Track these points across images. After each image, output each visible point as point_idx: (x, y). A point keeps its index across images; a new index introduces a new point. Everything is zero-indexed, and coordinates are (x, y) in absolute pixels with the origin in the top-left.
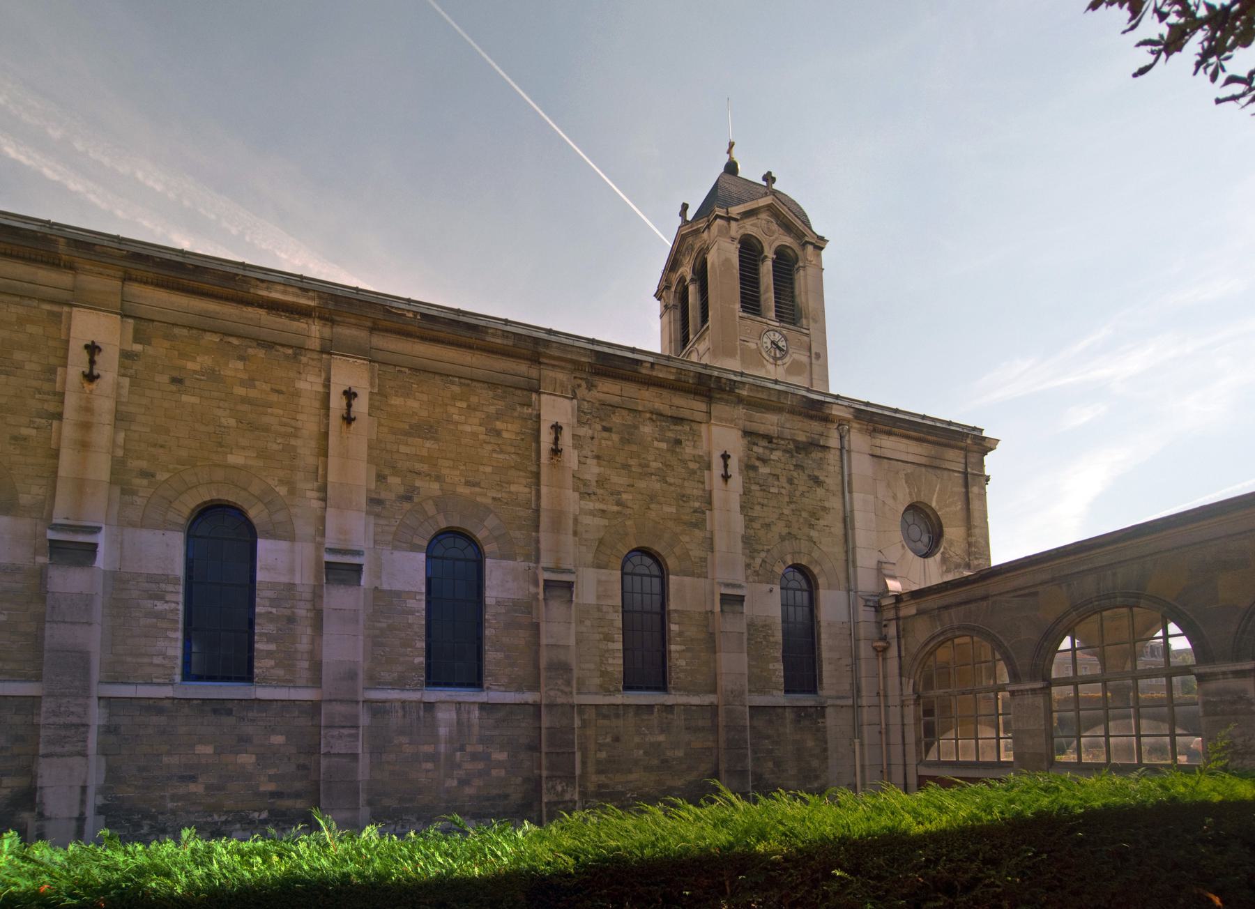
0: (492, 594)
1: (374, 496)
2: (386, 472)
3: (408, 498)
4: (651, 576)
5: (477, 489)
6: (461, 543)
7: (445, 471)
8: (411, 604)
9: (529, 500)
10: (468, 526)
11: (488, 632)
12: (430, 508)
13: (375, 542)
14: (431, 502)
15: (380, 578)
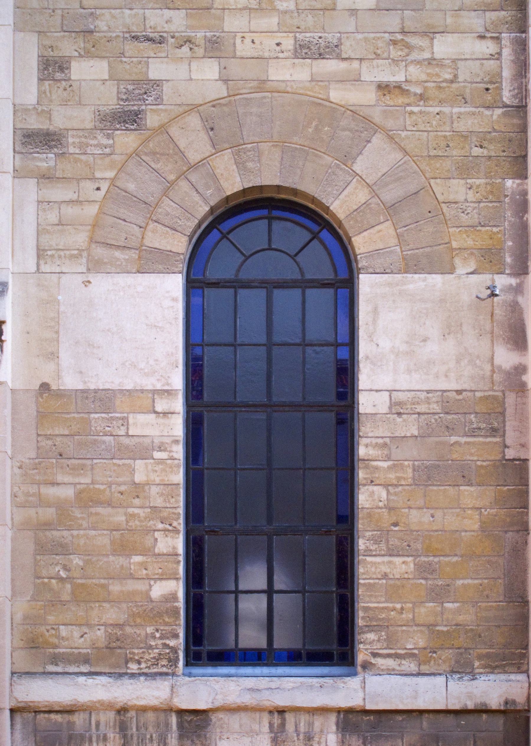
0: (375, 386)
1: (34, 123)
2: (68, 47)
3: (128, 118)
4: (304, 284)
5: (330, 66)
6: (290, 233)
7: (233, 23)
8: (143, 425)
9: (495, 79)
10: (308, 181)
11: (368, 497)
12: (194, 142)
13: (41, 254)
14: (194, 121)
15: (53, 356)
